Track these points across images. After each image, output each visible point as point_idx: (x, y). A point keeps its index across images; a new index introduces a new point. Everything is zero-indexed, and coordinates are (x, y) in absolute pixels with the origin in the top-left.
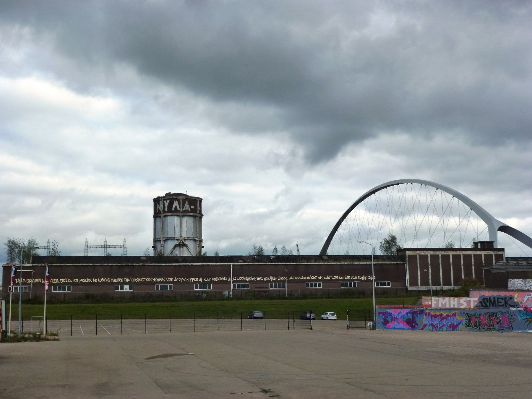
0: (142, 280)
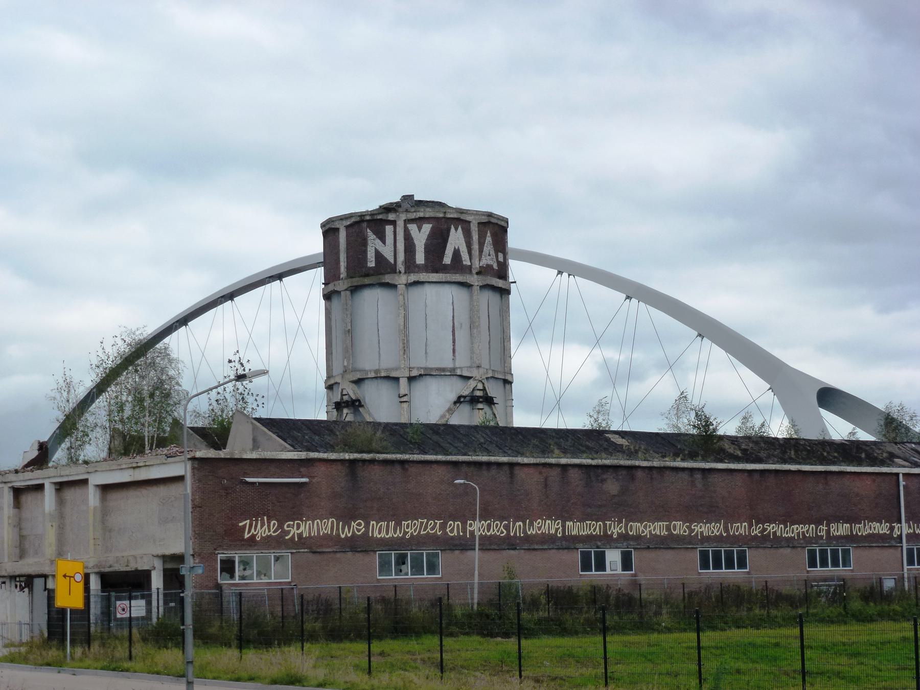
0: (658, 528)
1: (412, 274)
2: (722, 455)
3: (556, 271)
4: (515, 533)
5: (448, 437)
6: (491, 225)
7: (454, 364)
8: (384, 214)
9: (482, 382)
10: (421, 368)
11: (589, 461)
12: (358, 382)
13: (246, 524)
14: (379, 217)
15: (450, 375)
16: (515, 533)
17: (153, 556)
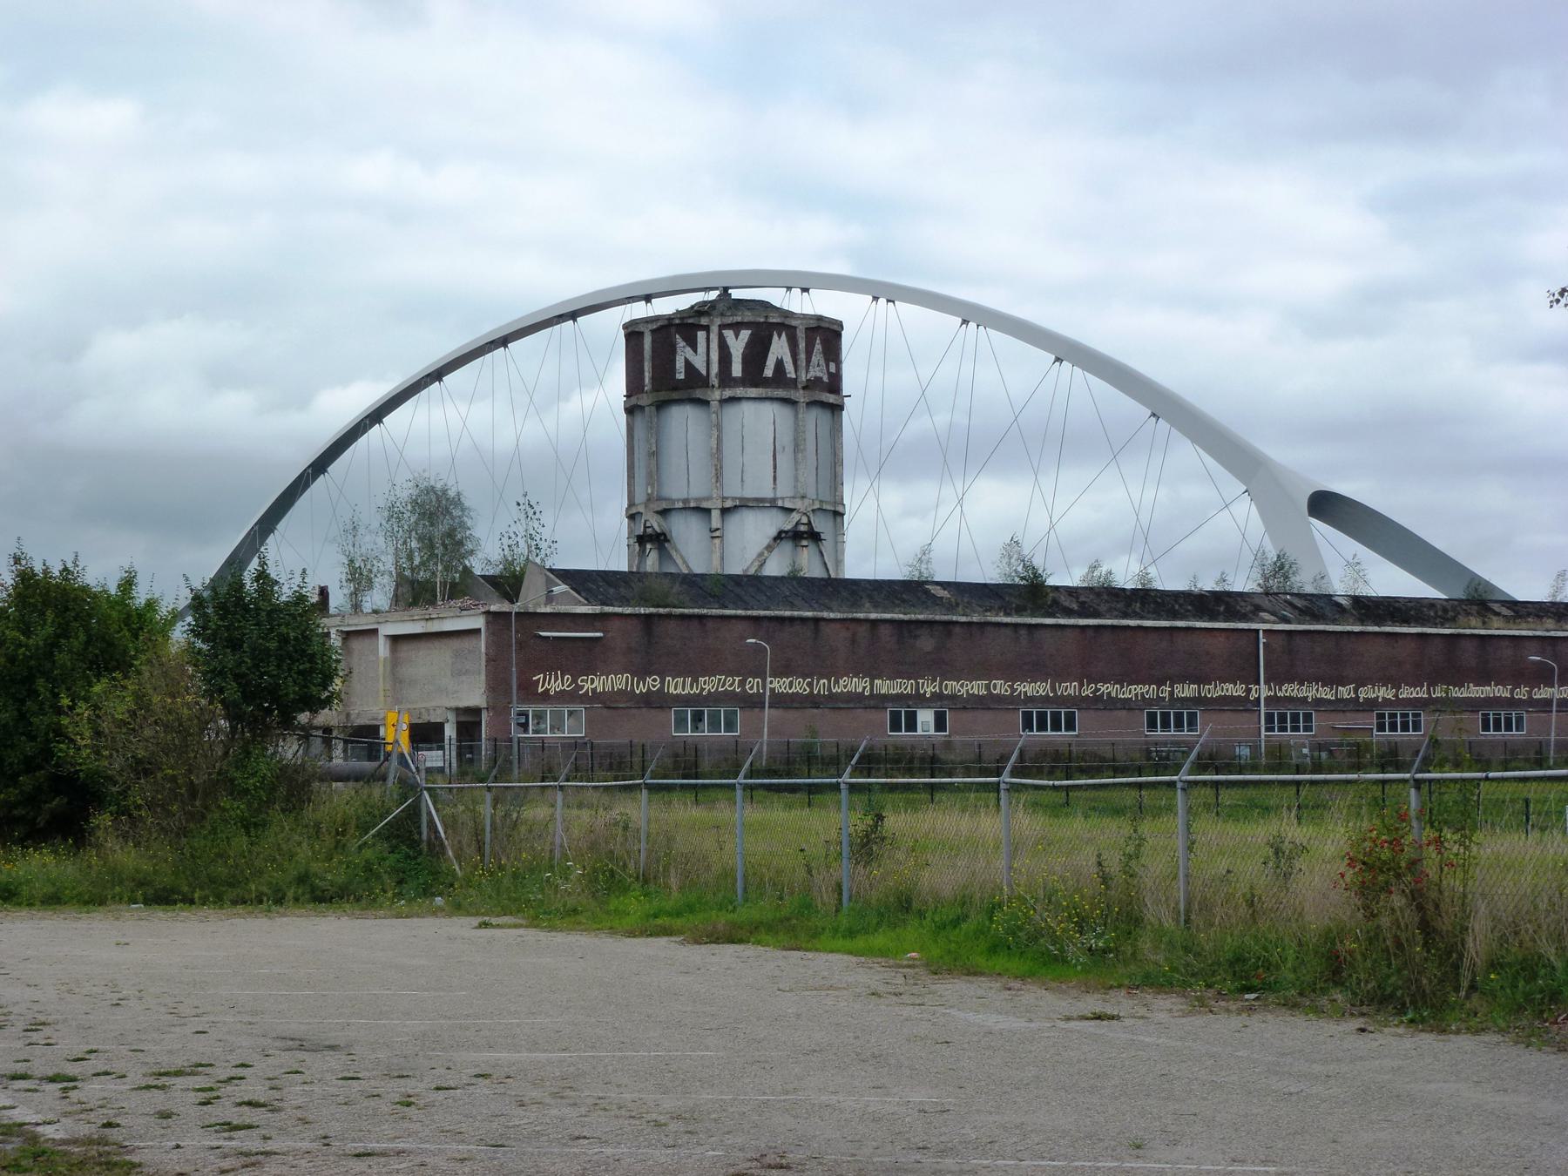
0: (976, 688)
1: (727, 389)
2: (1055, 608)
3: (960, 320)
4: (819, 691)
7: (775, 493)
10: (736, 498)
11: (901, 616)
12: (664, 513)
14: (690, 321)
16: (819, 691)
17: (446, 708)
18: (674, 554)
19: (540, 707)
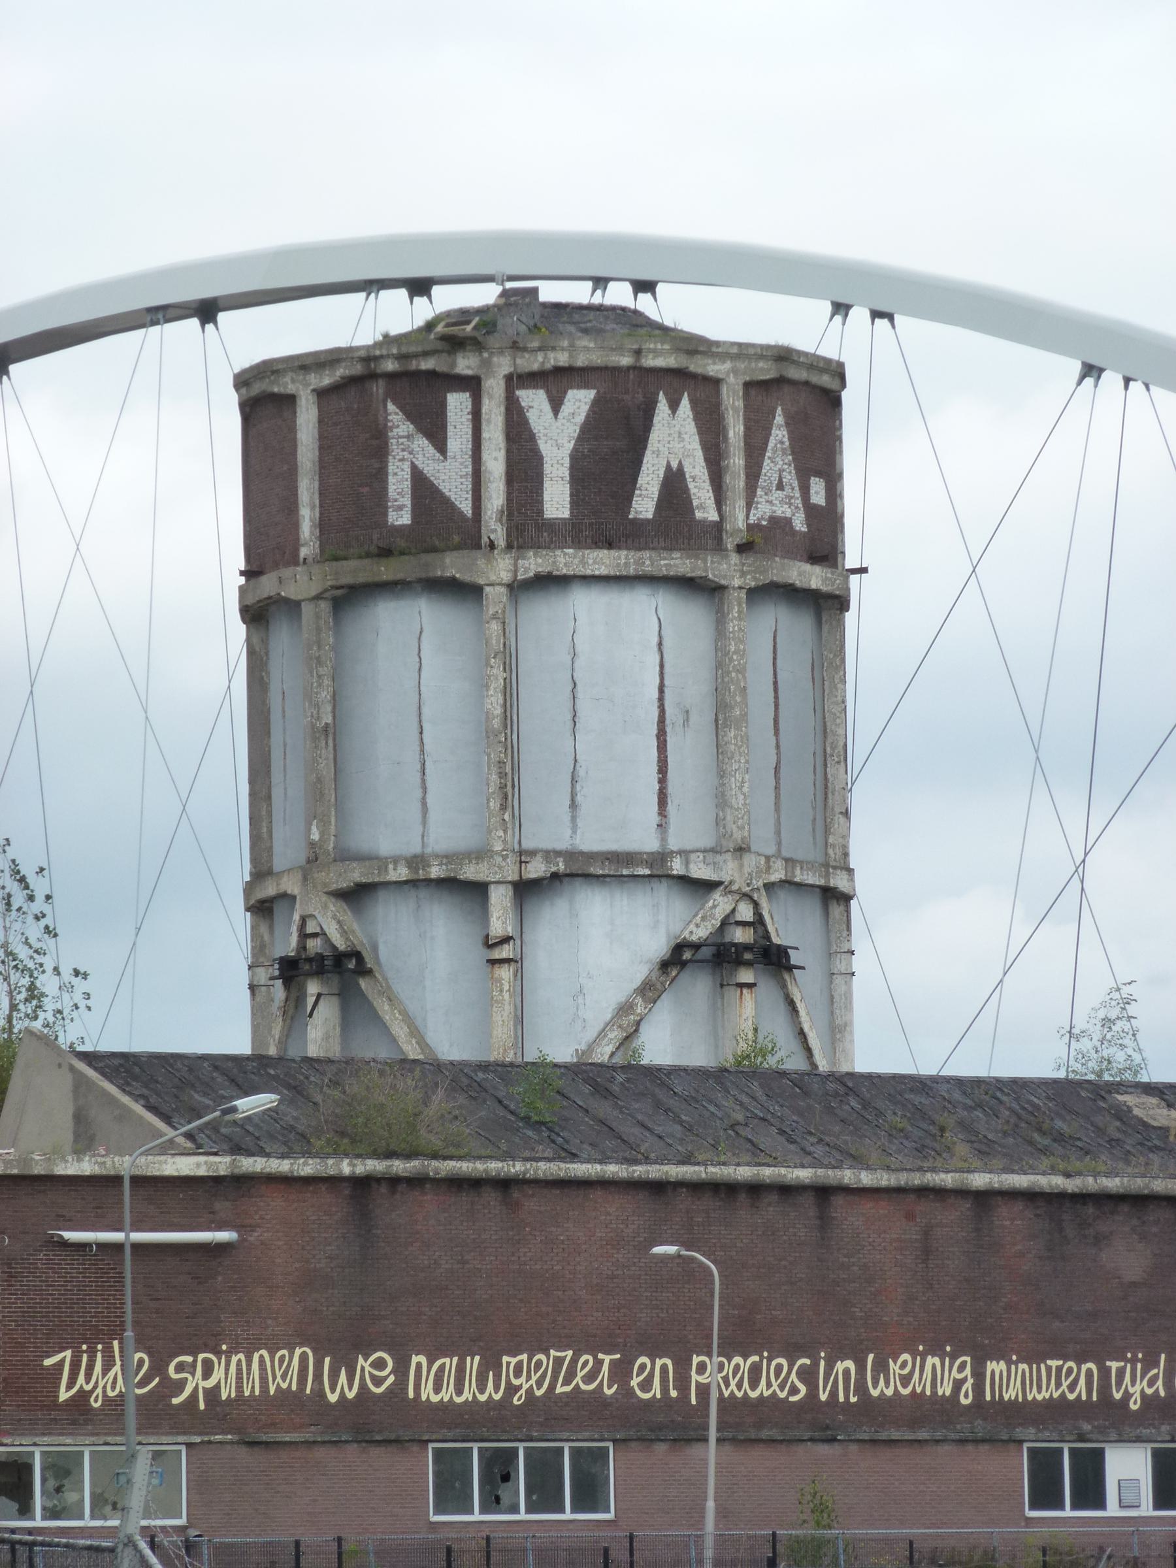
4: (834, 1394)
5: (637, 1106)
6: (787, 389)
7: (664, 839)
8: (445, 355)
9: (751, 898)
10: (558, 853)
11: (1057, 1182)
13: (63, 1360)
14: (427, 364)
15: (649, 876)
16: (834, 1394)
18: (384, 1008)
19: (65, 1443)
